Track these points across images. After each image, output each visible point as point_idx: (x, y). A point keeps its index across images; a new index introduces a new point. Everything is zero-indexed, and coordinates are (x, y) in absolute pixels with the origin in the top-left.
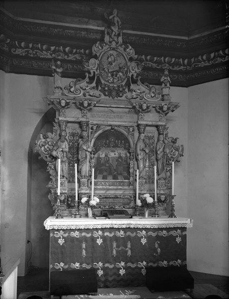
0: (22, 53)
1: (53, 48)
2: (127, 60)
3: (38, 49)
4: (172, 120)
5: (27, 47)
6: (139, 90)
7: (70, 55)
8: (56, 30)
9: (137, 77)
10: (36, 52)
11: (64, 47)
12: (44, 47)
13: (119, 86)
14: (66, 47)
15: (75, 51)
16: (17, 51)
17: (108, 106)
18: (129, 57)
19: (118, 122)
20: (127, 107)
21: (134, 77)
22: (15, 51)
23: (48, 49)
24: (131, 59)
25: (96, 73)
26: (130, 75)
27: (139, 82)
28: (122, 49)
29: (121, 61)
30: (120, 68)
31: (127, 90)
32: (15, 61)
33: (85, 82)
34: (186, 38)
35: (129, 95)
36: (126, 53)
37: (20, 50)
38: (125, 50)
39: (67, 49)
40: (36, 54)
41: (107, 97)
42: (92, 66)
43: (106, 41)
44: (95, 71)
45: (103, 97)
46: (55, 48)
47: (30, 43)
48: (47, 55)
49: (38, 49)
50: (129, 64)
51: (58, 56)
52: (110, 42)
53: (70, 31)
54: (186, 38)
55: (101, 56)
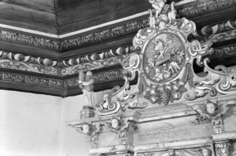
0: (71, 72)
1: (101, 55)
2: (184, 41)
3: (87, 61)
4: (190, 121)
5: (75, 63)
6: (207, 80)
7: (124, 56)
8: (102, 33)
9: (202, 60)
10: (86, 66)
11: (114, 50)
12: (92, 57)
13: (172, 84)
14: (117, 49)
15: (127, 50)
16: (67, 71)
17: (157, 118)
18: (186, 35)
19: (182, 140)
20: (189, 113)
21: (198, 62)
22: (64, 72)
23: (98, 58)
24: (191, 38)
25: (139, 73)
26: (191, 62)
27: (207, 68)
28: (175, 28)
29: (173, 44)
30: (172, 56)
31: (187, 86)
32: (70, 82)
33: (124, 90)
34: (55, 36)
35: (191, 92)
36: (181, 31)
37: (70, 68)
38: (179, 27)
39: (118, 51)
40: (86, 68)
41: (157, 105)
42: (132, 64)
43: (151, 25)
44: (137, 70)
45: (150, 105)
46: (104, 54)
47: (77, 58)
48: (98, 65)
49: (87, 61)
50: (187, 45)
51: (110, 62)
52: (157, 25)
53: (117, 28)
54: (55, 36)
55: (144, 47)
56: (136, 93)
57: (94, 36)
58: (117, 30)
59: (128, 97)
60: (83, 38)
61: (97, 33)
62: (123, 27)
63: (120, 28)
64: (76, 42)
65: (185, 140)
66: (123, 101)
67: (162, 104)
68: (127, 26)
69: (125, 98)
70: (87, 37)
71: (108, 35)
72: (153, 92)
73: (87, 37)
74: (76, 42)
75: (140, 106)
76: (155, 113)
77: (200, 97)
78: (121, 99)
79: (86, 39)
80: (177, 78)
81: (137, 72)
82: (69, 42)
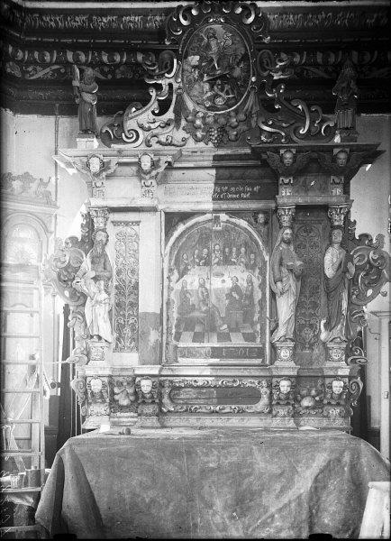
25: (175, 86)
53: (132, 18)
56: (169, 120)
57: (90, 20)
58: (130, 21)
59: (157, 124)
60: (69, 18)
61: (97, 15)
62: (141, 19)
63: (137, 18)
64: (56, 22)
65: (380, 363)
66: (149, 129)
67: (211, 145)
68: (149, 18)
69: (152, 126)
70: (77, 19)
71: (114, 25)
72: (198, 122)
73: (77, 19)
74: (56, 22)
75: (176, 143)
76: (42, 408)
77: (174, 145)
78: (147, 126)
79: (75, 21)
80: (114, 273)
81: (170, 85)
82: (42, 20)
